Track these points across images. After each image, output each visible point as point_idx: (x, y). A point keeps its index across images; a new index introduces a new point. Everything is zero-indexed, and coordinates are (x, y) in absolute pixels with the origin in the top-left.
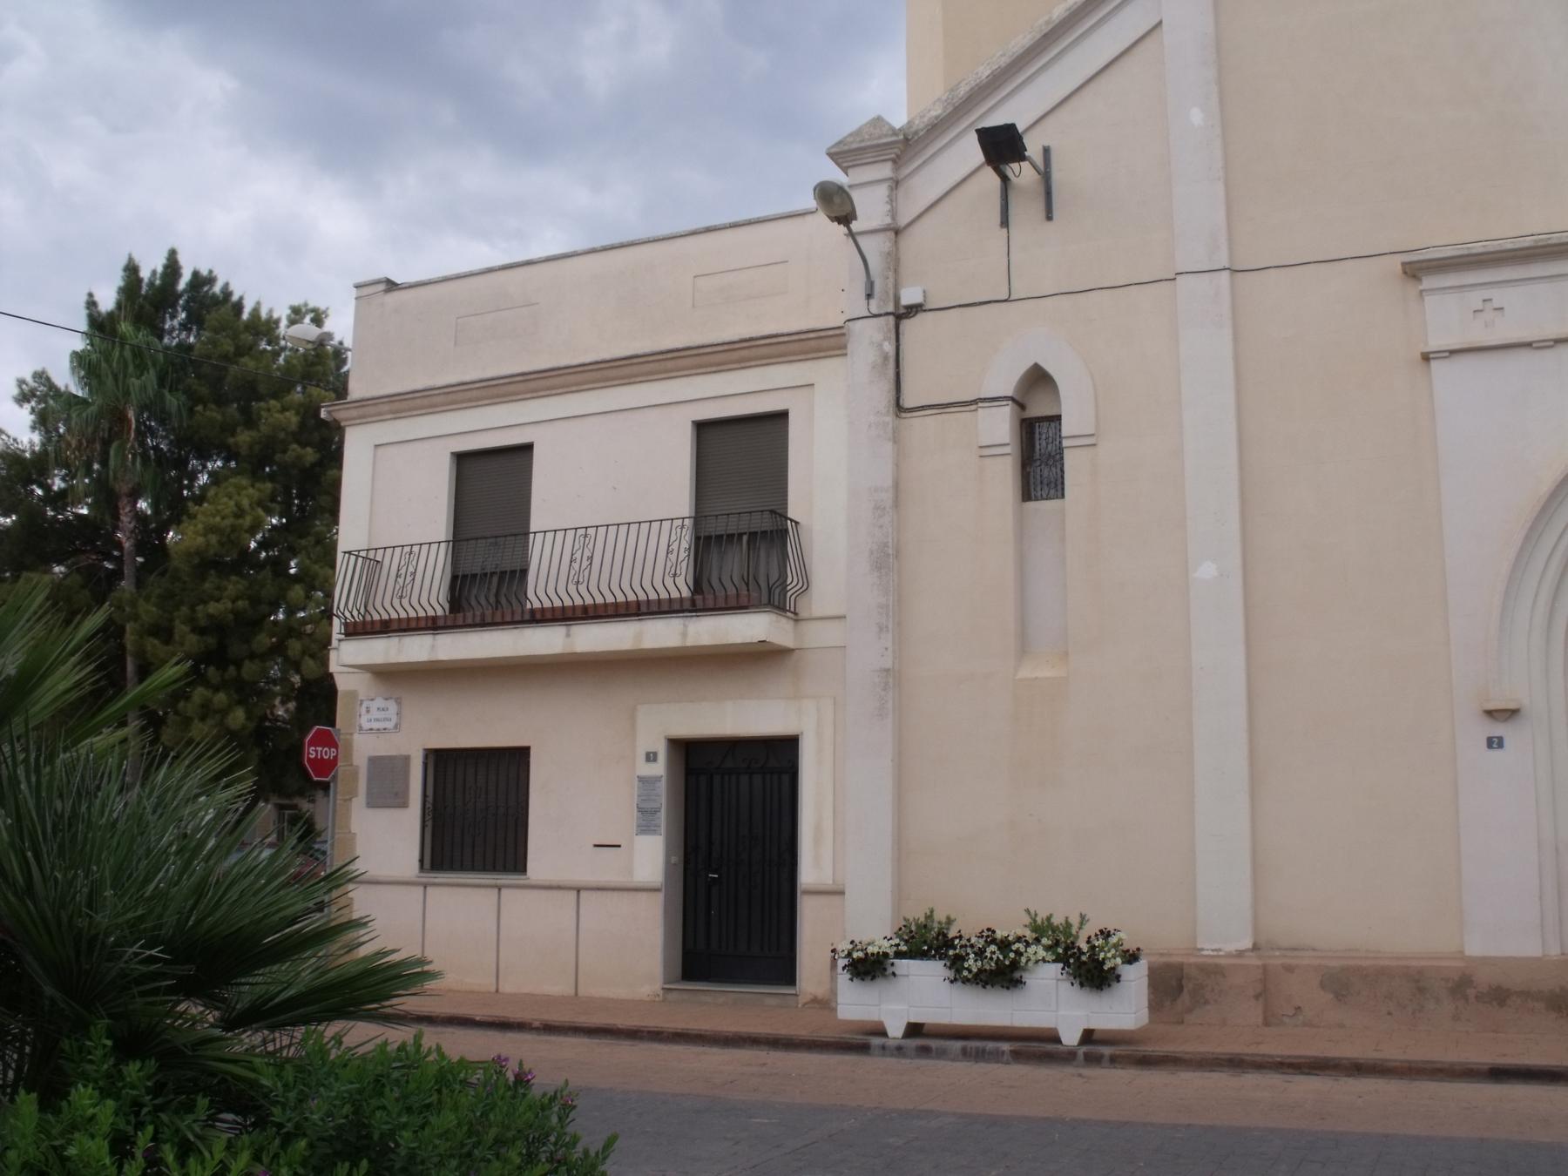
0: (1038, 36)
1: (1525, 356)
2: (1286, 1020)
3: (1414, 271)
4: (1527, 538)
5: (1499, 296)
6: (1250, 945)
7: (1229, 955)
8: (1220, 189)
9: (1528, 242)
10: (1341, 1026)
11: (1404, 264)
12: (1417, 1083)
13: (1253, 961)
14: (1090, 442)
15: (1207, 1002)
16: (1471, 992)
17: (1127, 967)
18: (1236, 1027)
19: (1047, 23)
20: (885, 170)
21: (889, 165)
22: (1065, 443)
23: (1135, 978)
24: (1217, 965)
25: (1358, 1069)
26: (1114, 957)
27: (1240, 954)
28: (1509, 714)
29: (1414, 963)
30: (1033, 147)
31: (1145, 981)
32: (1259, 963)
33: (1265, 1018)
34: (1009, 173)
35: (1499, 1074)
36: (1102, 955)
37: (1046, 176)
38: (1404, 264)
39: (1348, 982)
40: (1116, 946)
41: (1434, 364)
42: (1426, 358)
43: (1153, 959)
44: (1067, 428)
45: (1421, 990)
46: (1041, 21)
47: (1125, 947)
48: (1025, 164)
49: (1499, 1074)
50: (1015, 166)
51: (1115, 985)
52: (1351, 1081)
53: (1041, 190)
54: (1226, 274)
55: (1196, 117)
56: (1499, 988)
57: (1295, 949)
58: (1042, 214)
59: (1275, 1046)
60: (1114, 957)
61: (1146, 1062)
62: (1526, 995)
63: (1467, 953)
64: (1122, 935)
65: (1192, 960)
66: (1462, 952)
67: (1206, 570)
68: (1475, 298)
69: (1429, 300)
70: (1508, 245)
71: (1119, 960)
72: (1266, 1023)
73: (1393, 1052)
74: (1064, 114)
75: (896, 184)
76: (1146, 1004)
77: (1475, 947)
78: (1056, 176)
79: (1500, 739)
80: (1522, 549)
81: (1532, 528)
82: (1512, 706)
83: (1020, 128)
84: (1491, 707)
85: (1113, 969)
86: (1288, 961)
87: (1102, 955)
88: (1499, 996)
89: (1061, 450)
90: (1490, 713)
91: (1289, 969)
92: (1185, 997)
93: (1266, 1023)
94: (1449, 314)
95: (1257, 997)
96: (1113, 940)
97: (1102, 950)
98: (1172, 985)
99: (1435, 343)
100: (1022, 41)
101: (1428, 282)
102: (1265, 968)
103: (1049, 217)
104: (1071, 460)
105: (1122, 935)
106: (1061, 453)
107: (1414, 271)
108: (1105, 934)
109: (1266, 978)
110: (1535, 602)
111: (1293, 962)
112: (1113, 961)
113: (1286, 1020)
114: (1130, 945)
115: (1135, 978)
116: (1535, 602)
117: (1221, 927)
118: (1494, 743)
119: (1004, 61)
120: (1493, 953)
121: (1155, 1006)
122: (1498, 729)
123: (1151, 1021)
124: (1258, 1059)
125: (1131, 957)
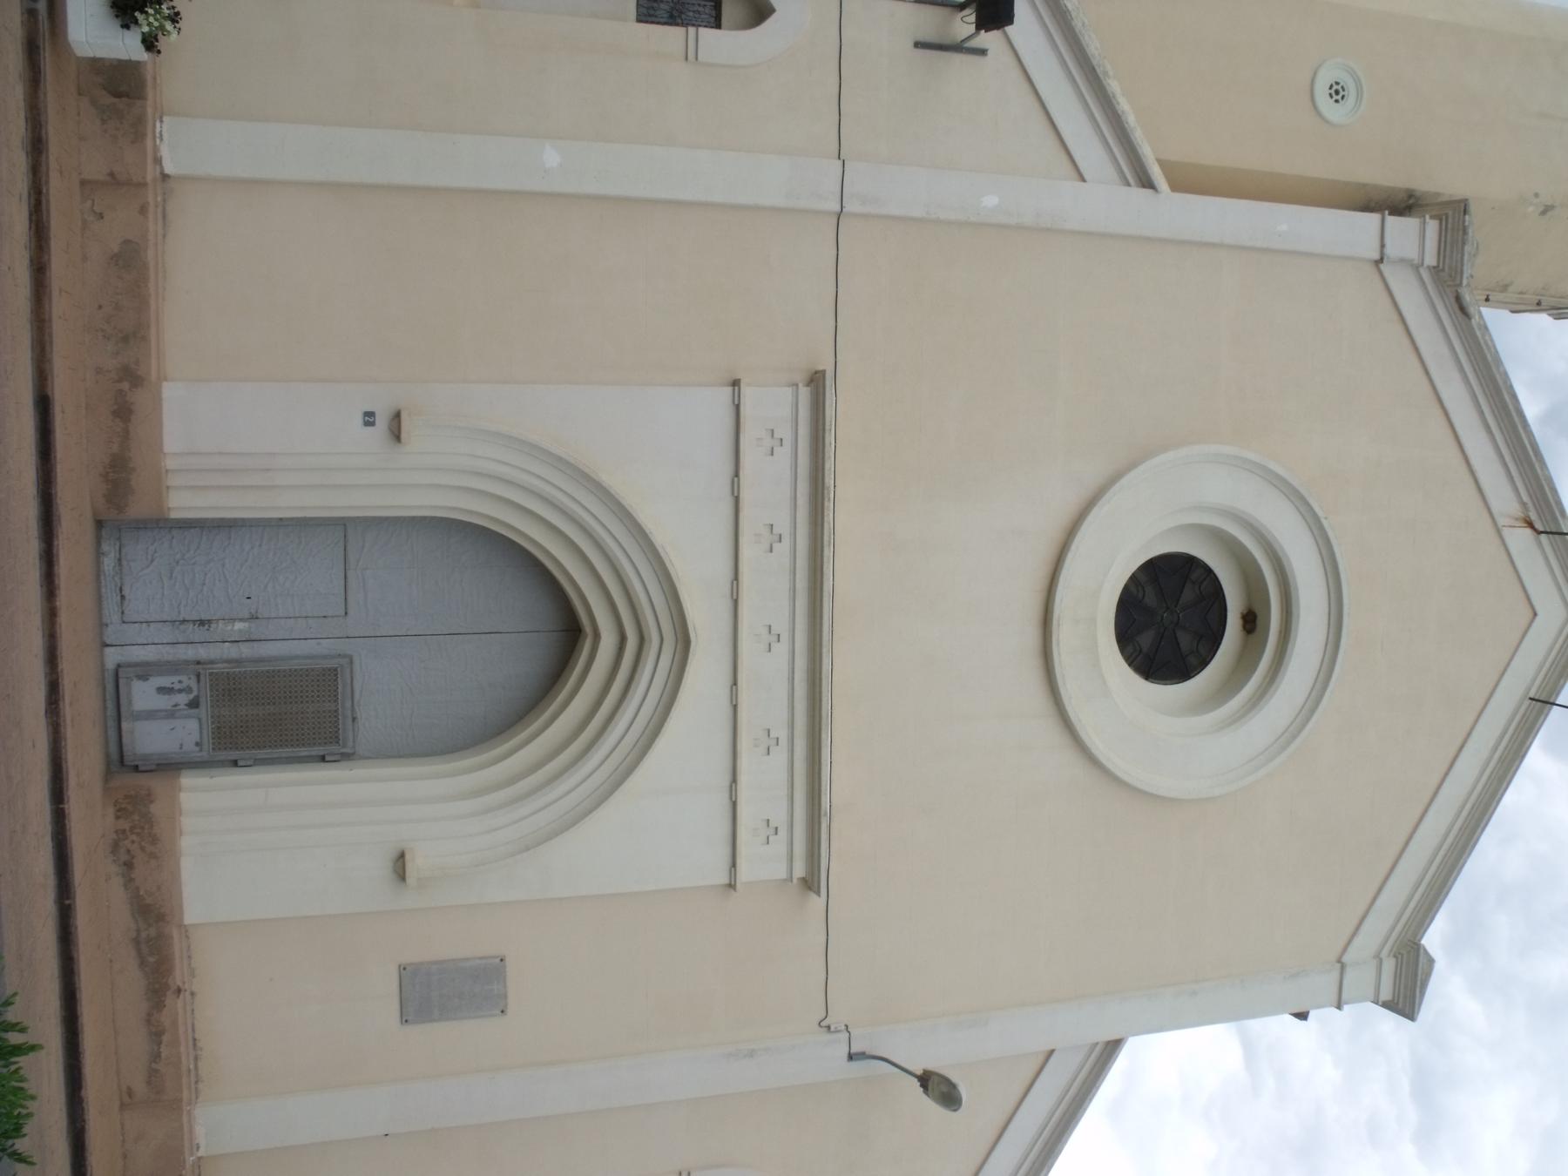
0: (1095, 63)
1: (728, 469)
2: (89, 203)
3: (816, 381)
4: (560, 459)
5: (784, 453)
6: (167, 171)
7: (156, 149)
8: (917, 213)
9: (829, 481)
10: (85, 258)
11: (824, 372)
12: (28, 326)
13: (151, 173)
14: (690, 56)
15: (104, 122)
16: (125, 386)
17: (139, 38)
18: (77, 149)
19: (1106, 73)
20: (1431, 259)
21: (1434, 263)
22: (692, 30)
23: (125, 45)
24: (144, 135)
25: (39, 270)
26: (149, 24)
27: (158, 161)
28: (396, 434)
29: (153, 331)
30: (989, 39)
31: (123, 56)
32: (149, 178)
33: (89, 182)
34: (967, 11)
35: (44, 405)
36: (151, 11)
37: (958, 48)
38: (824, 372)
39: (131, 267)
40: (162, 28)
41: (730, 389)
42: (736, 383)
43: (149, 67)
44: (707, 34)
45: (125, 339)
46: (1109, 67)
47: (160, 36)
48: (972, 28)
49: (44, 405)
50: (973, 18)
51: (118, 23)
52: (26, 262)
53: (947, 41)
54: (838, 208)
55: (991, 201)
56: (130, 411)
57: (164, 217)
58: (921, 38)
59: (57, 187)
60: (149, 24)
61: (32, 49)
62: (126, 436)
63: (165, 384)
64: (174, 35)
65: (150, 110)
66: (166, 379)
67: (551, 157)
68: (785, 432)
69: (789, 391)
70: (829, 465)
71: (146, 29)
72: (83, 183)
73: (59, 306)
74: (1016, 73)
75: (1416, 268)
76: (99, 54)
77: (171, 393)
78: (957, 58)
79: (372, 424)
80: (550, 454)
81: (568, 463)
82: (404, 436)
83: (1008, 29)
84: (404, 416)
85: (136, 22)
86: (151, 209)
87: (151, 11)
88: (123, 412)
89: (685, 24)
90: (398, 415)
91: (143, 210)
92: (110, 100)
93: (83, 183)
94: (773, 407)
95: (112, 174)
96: (169, 26)
97: (157, 12)
98: (121, 87)
99: (748, 392)
100: (1093, 46)
101: (805, 393)
102: (145, 185)
103: (917, 45)
104: (674, 34)
105: (174, 35)
106: (682, 25)
107: (816, 381)
108: (175, 18)
109: (133, 186)
110: (539, 477)
111: (151, 216)
112: (147, 21)
113: (89, 203)
114: (162, 43)
115: (125, 45)
116: (539, 477)
117: (184, 144)
118: (369, 418)
119: (1077, 24)
120: (166, 407)
121: (98, 66)
122: (382, 421)
123: (80, 60)
124: (44, 168)
125: (150, 43)
